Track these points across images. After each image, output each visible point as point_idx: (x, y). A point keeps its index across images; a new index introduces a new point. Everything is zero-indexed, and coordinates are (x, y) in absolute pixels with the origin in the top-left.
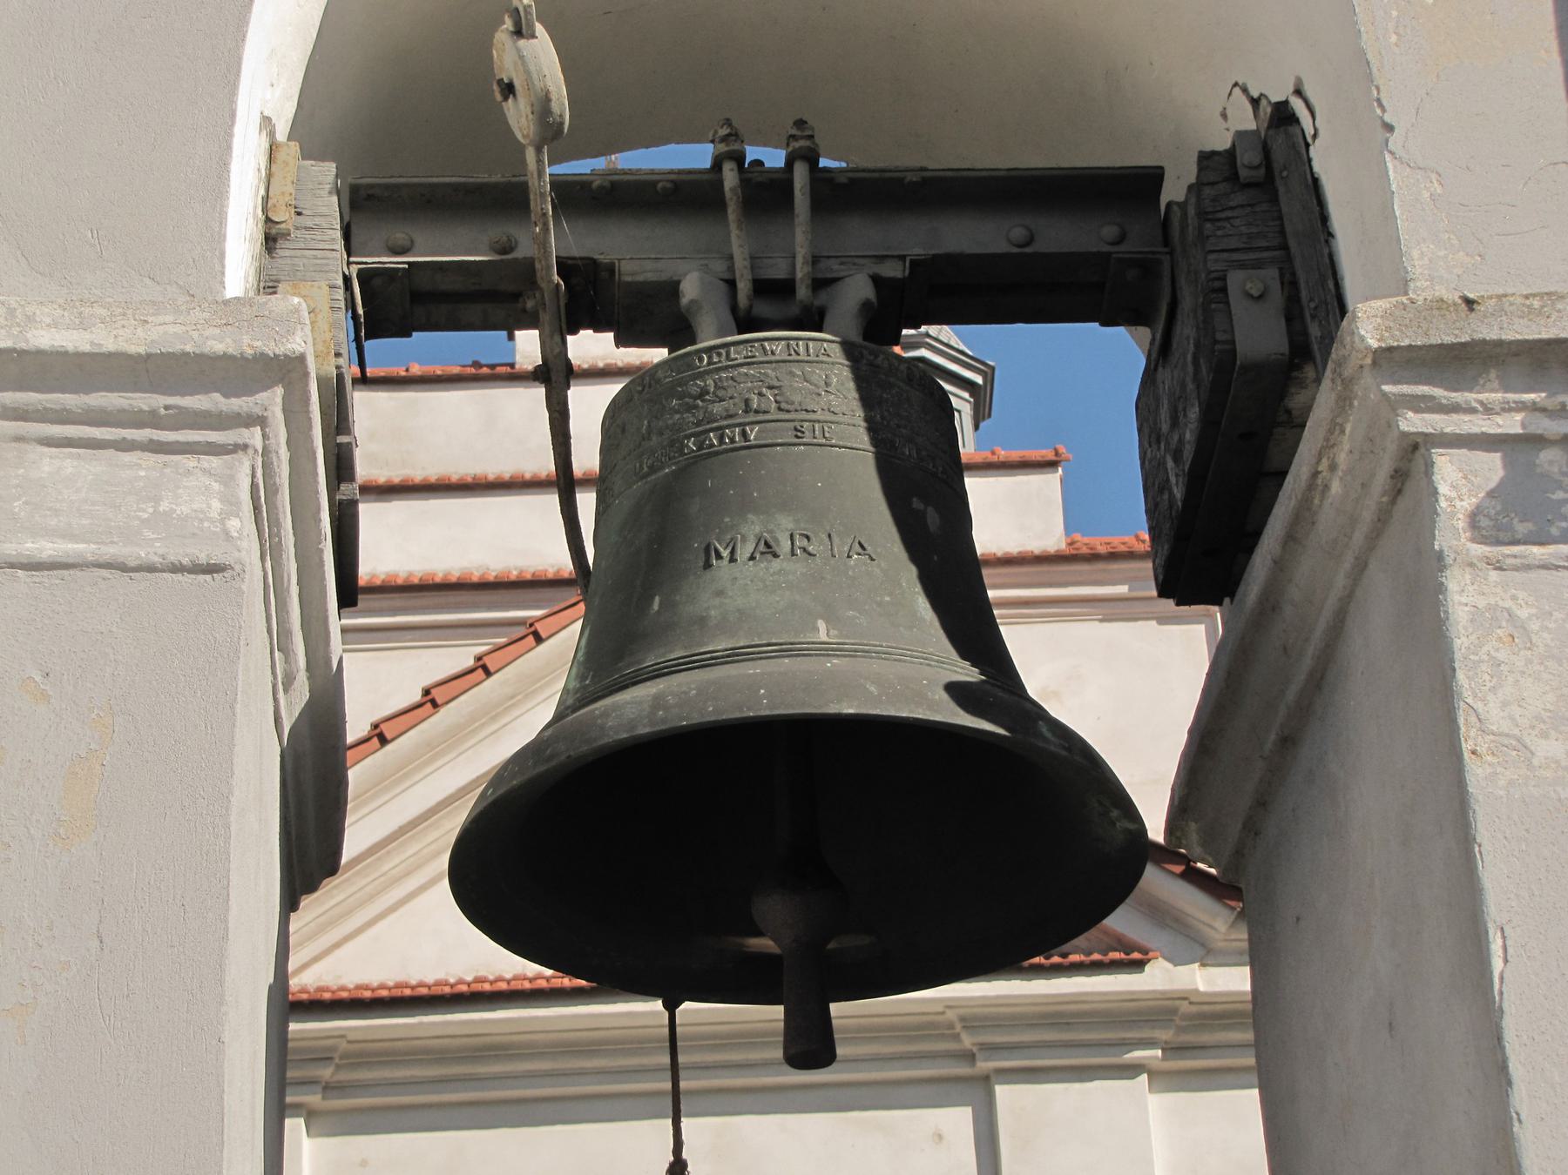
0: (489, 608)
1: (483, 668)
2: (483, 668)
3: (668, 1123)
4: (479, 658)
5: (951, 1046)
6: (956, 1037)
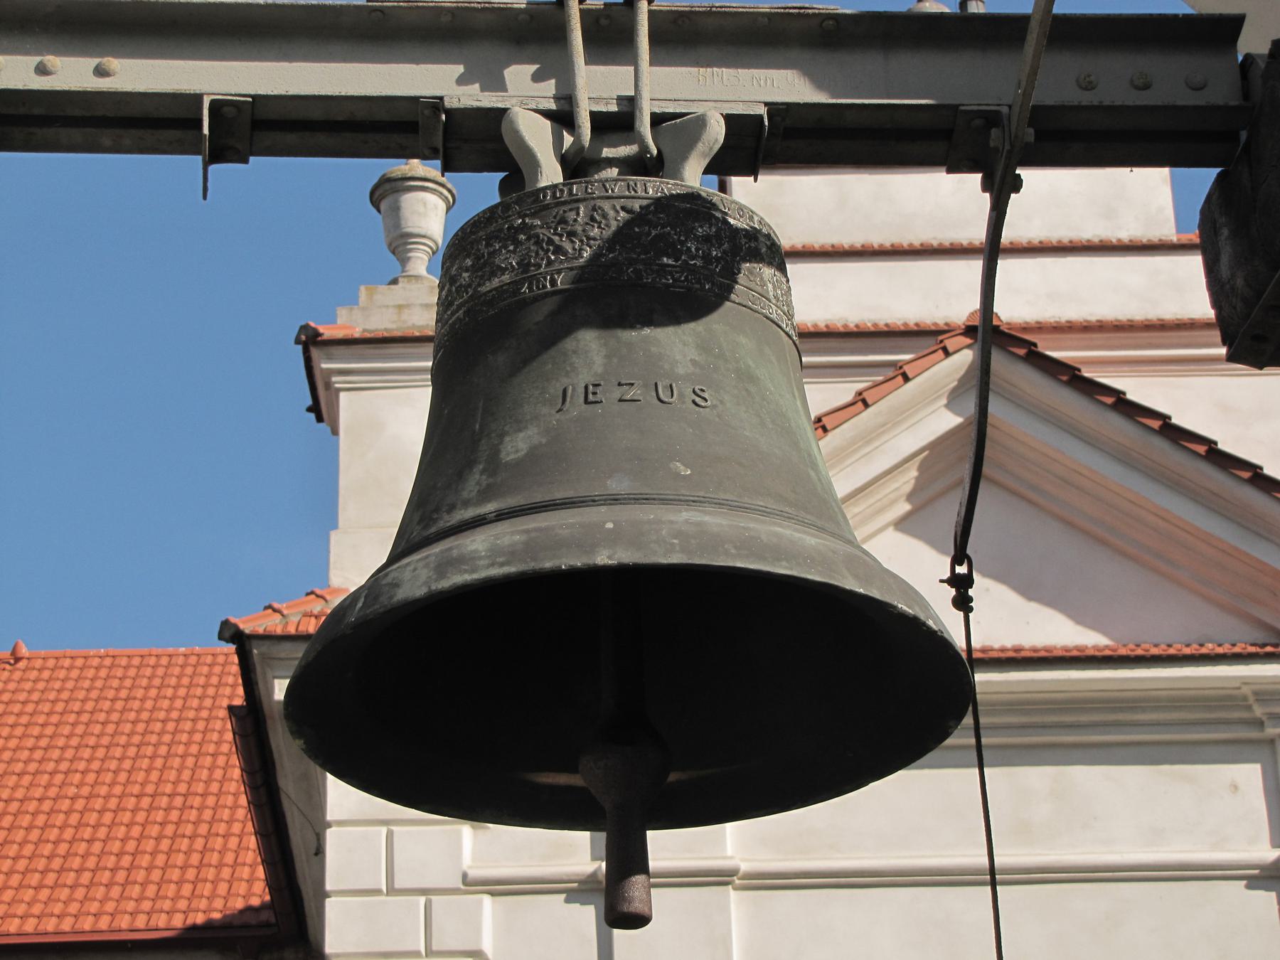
0: (852, 352)
1: (862, 401)
2: (862, 401)
3: (977, 771)
4: (860, 394)
5: (1245, 715)
6: (1249, 708)
